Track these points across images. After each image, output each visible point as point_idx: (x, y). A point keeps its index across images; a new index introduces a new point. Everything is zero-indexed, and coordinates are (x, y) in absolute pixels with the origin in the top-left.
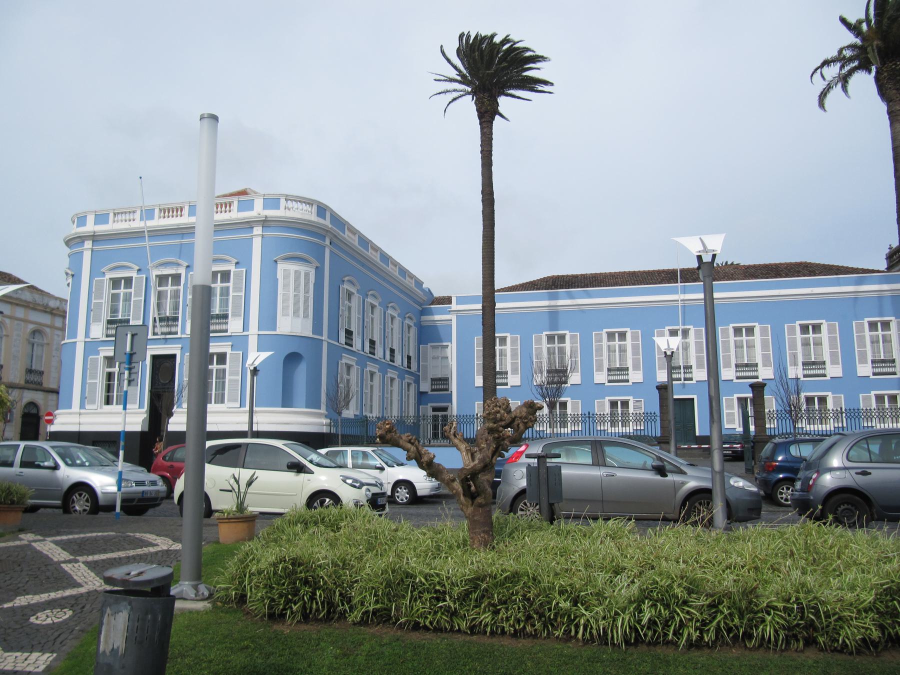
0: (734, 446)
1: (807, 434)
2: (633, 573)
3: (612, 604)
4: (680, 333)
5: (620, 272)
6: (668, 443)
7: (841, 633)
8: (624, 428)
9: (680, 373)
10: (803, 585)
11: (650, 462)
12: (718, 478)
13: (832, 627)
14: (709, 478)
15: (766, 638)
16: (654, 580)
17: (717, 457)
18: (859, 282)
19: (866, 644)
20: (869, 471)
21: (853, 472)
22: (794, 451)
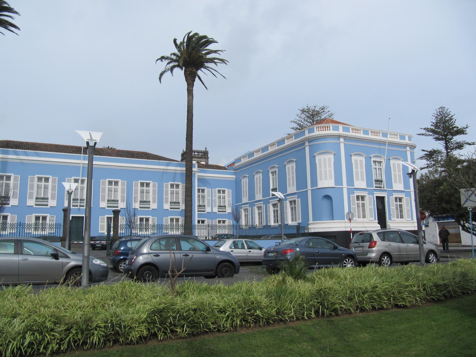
0: (102, 242)
1: (139, 236)
2: (24, 317)
3: (7, 336)
4: (80, 181)
5: (49, 144)
6: (65, 240)
7: (130, 335)
8: (140, 232)
9: (78, 202)
10: (115, 313)
11: (51, 251)
12: (86, 259)
13: (126, 333)
14: (81, 260)
15: (94, 343)
16: (35, 319)
17: (86, 248)
18: (168, 165)
19: (142, 339)
20: (159, 254)
21: (152, 255)
22: (129, 245)
